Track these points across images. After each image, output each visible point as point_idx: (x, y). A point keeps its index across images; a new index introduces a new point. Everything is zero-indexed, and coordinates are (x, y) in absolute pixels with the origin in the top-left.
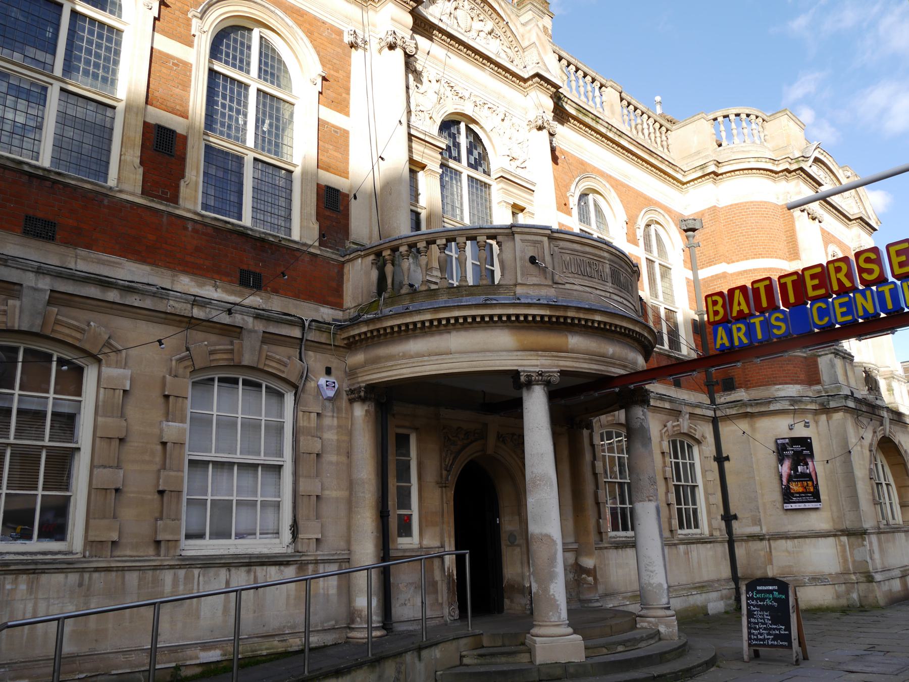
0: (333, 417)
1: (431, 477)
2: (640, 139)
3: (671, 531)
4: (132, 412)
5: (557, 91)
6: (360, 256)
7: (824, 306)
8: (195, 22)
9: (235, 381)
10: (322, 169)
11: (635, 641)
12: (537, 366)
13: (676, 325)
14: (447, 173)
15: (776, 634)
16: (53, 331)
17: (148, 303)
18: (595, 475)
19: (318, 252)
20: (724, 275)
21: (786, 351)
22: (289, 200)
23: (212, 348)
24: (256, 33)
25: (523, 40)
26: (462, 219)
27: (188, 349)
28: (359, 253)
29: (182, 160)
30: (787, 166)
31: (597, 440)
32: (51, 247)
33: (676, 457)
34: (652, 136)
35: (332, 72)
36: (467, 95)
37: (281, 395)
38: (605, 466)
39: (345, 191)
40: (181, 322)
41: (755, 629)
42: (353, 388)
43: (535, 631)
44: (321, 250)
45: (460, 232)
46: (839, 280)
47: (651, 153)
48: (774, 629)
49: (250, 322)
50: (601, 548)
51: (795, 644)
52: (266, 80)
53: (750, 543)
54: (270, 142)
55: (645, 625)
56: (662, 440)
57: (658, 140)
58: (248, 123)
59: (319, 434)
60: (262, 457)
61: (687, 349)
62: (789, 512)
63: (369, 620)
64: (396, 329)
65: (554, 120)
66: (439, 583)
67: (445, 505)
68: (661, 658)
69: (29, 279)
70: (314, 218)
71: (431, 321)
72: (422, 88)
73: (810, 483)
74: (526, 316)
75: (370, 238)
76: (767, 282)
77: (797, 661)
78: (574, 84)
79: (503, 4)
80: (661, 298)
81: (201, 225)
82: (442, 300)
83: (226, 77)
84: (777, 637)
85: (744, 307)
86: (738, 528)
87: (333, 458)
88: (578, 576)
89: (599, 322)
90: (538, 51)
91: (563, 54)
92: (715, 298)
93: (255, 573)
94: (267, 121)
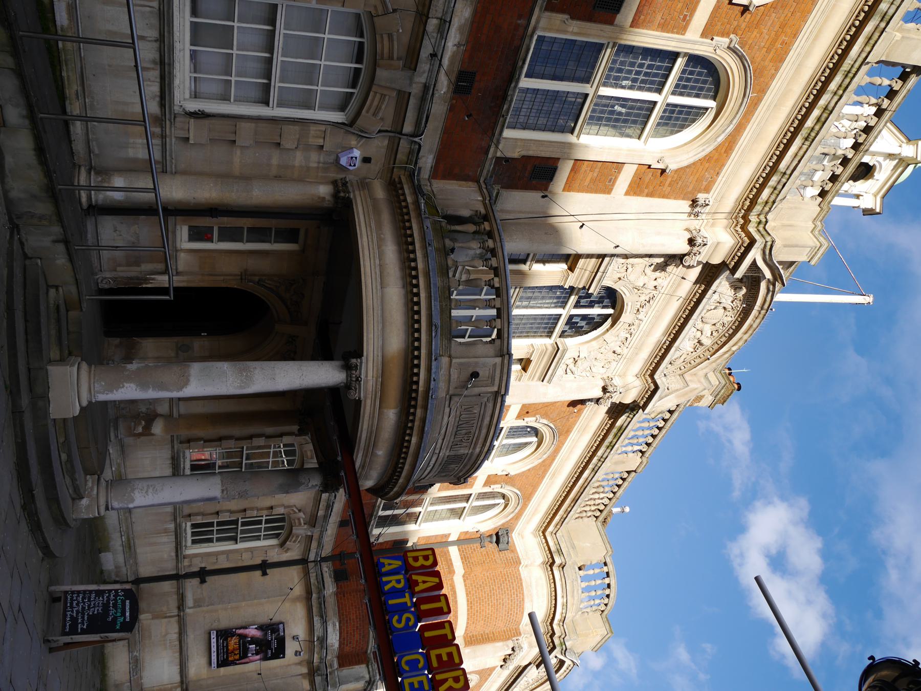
0: (319, 163)
1: (252, 264)
2: (590, 490)
3: (190, 515)
5: (640, 408)
6: (484, 199)
7: (420, 666)
9: (359, 60)
10: (574, 165)
11: (72, 473)
12: (367, 376)
13: (402, 523)
14: (561, 294)
15: (78, 619)
16: (376, 93)
18: (251, 437)
19: (490, 156)
20: (452, 572)
21: (375, 629)
22: (544, 129)
23: (395, 37)
24: (711, 104)
25: (691, 375)
26: (518, 307)
27: (395, 11)
28: (488, 198)
29: (590, 18)
30: (557, 634)
31: (287, 440)
33: (267, 522)
34: (592, 502)
35: (669, 180)
36: (641, 316)
37: (342, 108)
38: (259, 447)
39: (551, 187)
40: (424, 5)
41: (83, 598)
42: (349, 185)
43: (84, 366)
44: (492, 159)
45: (505, 302)
46: (446, 680)
47: (575, 500)
48: (83, 618)
49: (421, 79)
50: (172, 441)
51: (67, 639)
52: (665, 111)
53: (175, 597)
54: (602, 112)
55: (90, 484)
56: (285, 507)
57: (587, 508)
58: (622, 91)
59: (300, 146)
60: (278, 85)
61: (380, 534)
62: (207, 636)
63: (99, 189)
64: (409, 232)
65: (612, 403)
66: (138, 269)
67: (222, 278)
68: (53, 499)
70: (524, 153)
71: (416, 269)
72: (649, 271)
73: (237, 657)
74: (418, 366)
75: (502, 211)
76: (445, 610)
77: (49, 641)
78: (646, 425)
79: (727, 355)
80: (431, 508)
81: (520, 35)
82: (437, 281)
83: (670, 69)
84: (74, 620)
85: (422, 586)
86: (191, 585)
87: (275, 161)
88: (141, 416)
89: (409, 441)
90: (680, 389)
91: (676, 415)
92: (431, 558)
93: (153, 69)
94: (624, 110)
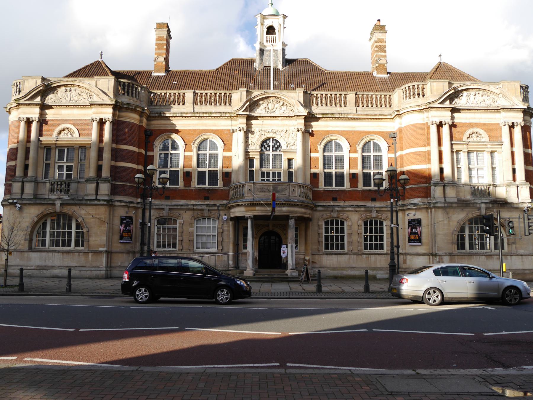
4: (184, 227)
8: (193, 146)
17: (185, 208)
32: (169, 201)
69: (165, 207)
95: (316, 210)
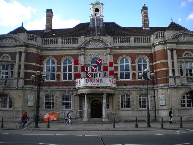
17: (57, 90)
95: (117, 90)
